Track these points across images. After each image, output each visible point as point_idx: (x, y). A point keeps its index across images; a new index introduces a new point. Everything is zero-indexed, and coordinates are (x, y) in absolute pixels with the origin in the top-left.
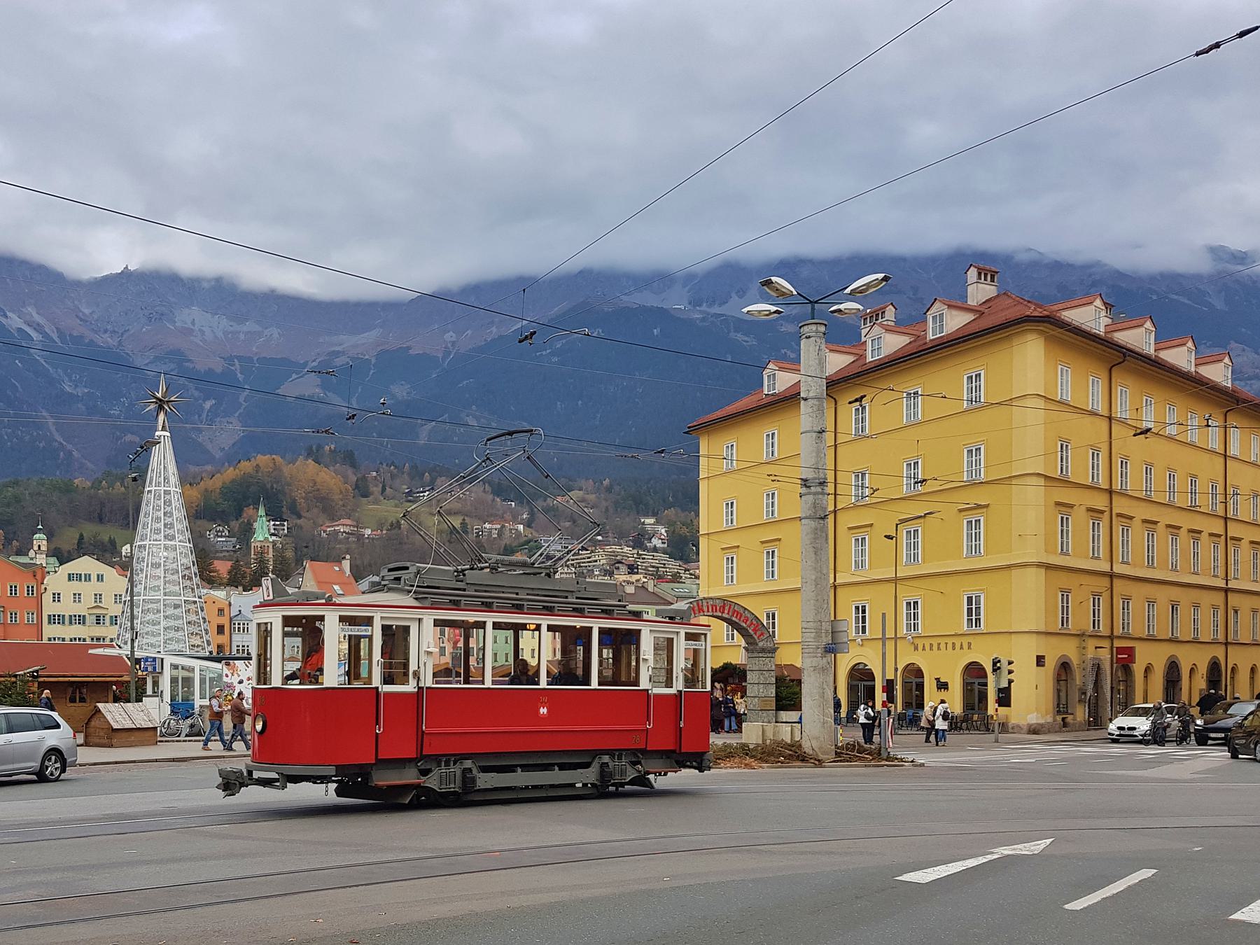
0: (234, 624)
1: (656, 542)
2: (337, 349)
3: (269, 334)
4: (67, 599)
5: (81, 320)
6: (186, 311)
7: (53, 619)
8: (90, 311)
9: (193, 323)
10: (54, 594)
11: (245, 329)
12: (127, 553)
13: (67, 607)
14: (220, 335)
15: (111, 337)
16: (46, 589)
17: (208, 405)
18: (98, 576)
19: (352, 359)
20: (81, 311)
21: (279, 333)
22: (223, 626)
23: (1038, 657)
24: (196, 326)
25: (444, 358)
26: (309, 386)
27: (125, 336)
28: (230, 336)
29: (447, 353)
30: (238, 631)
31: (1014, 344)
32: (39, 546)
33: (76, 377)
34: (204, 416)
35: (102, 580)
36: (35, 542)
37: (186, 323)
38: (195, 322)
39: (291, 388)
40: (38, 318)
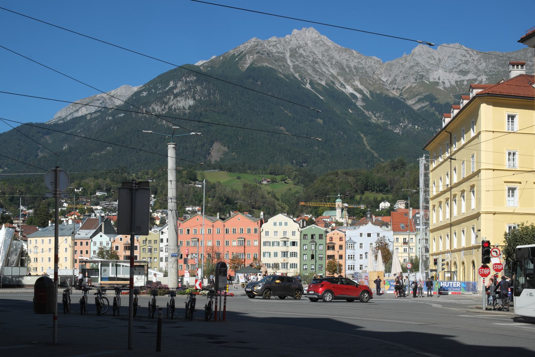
0: (347, 245)
3: (480, 80)
4: (271, 234)
6: (436, 72)
7: (265, 243)
8: (386, 80)
9: (439, 79)
12: (382, 207)
13: (271, 238)
15: (396, 92)
16: (263, 230)
20: (381, 80)
21: (486, 78)
24: (440, 80)
30: (351, 248)
33: (378, 115)
37: (435, 79)
38: (440, 78)
40: (360, 86)
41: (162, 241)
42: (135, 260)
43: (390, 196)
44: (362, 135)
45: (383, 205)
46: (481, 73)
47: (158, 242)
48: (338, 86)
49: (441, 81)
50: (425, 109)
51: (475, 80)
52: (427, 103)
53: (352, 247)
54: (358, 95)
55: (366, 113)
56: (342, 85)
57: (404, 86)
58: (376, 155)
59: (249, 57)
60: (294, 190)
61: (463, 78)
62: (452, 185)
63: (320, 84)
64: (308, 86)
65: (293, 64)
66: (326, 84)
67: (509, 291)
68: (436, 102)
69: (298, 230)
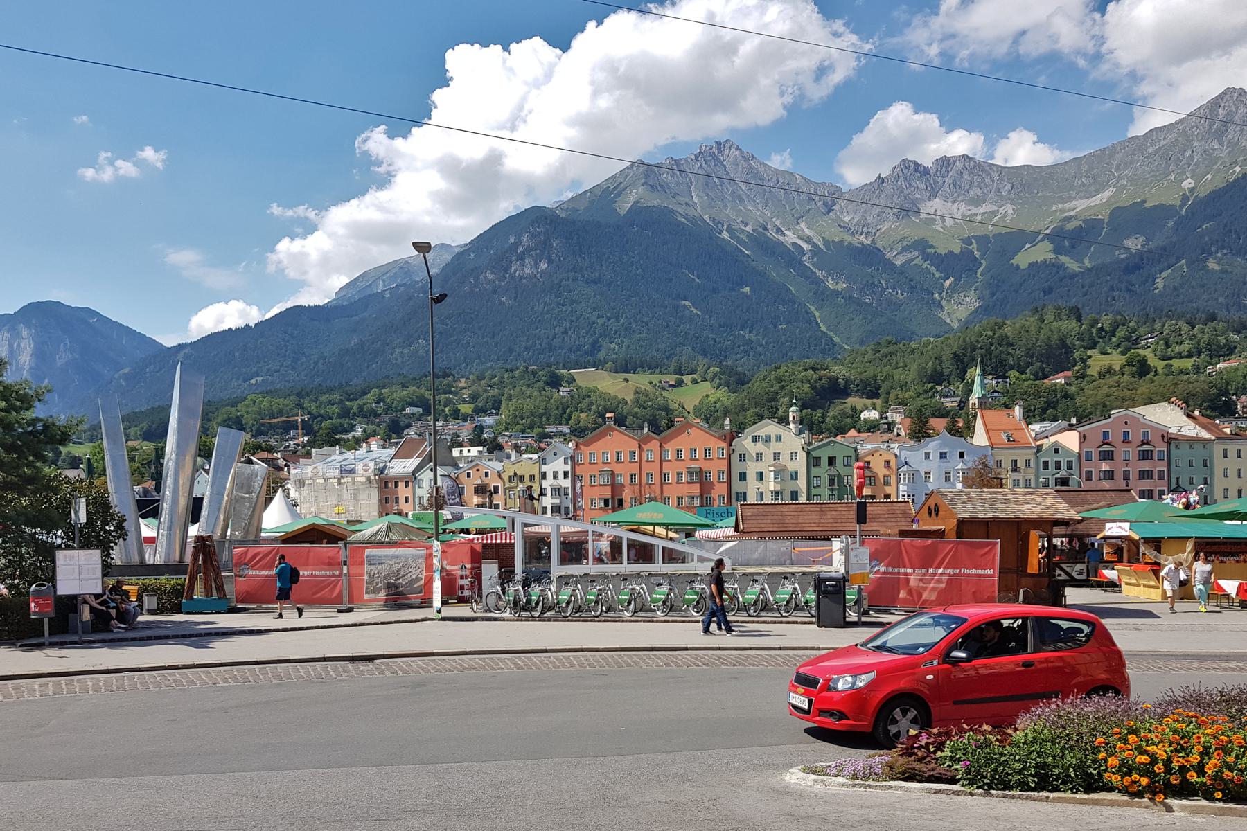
3: (1004, 212)
5: (841, 227)
10: (740, 455)
11: (981, 210)
17: (947, 284)
18: (777, 436)
21: (1013, 209)
23: (745, 480)
25: (1182, 206)
26: (1041, 252)
29: (1185, 198)
32: (794, 417)
34: (944, 293)
35: (780, 440)
36: (790, 414)
41: (544, 476)
43: (878, 402)
44: (813, 309)
45: (867, 416)
47: (537, 478)
48: (772, 233)
51: (995, 213)
52: (917, 254)
53: (909, 478)
54: (805, 246)
55: (818, 273)
56: (778, 230)
57: (879, 227)
58: (836, 339)
59: (631, 192)
60: (712, 399)
63: (743, 231)
64: (725, 235)
65: (701, 200)
66: (753, 230)
68: (933, 251)
69: (803, 448)
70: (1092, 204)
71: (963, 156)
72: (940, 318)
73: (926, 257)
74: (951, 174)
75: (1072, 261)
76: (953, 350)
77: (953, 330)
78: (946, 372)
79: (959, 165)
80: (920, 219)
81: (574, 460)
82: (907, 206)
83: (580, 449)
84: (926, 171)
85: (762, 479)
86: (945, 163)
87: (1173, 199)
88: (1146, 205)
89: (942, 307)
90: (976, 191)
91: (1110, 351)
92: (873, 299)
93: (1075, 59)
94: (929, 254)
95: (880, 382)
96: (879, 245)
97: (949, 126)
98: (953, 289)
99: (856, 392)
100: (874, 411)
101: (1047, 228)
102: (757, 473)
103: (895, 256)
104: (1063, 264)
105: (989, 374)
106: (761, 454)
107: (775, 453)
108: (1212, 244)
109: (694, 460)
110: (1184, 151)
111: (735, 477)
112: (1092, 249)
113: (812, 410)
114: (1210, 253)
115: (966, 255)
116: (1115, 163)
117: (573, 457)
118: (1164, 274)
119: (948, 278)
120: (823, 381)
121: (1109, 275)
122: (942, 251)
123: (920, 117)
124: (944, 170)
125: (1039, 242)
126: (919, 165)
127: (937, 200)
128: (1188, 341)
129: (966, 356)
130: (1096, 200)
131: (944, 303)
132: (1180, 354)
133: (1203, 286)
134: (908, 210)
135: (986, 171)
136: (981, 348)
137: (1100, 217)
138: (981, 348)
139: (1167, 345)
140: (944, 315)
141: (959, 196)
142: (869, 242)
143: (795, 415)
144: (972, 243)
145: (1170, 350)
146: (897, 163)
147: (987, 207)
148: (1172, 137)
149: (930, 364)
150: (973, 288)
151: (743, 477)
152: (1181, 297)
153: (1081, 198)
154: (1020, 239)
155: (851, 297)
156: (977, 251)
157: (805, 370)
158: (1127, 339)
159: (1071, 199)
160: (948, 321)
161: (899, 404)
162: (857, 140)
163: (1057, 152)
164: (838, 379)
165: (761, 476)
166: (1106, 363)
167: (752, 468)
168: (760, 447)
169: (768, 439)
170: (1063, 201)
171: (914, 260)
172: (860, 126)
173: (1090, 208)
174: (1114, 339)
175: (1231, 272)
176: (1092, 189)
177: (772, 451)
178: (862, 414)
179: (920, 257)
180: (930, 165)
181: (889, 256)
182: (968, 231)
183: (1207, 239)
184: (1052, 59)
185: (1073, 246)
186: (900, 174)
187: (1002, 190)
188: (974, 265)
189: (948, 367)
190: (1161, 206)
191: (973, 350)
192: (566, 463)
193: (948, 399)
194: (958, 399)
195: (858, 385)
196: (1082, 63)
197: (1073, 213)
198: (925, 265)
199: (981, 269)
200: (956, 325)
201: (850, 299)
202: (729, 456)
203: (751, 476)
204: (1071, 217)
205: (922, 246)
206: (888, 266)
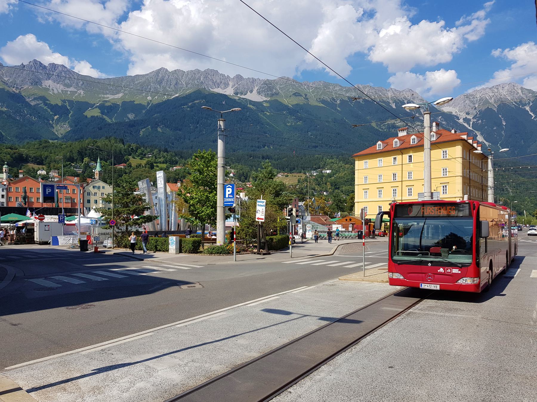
1: (231, 175)
2: (106, 99)
5: (3, 82)
9: (49, 86)
14: (60, 91)
15: (16, 90)
16: (85, 191)
17: (56, 117)
18: (103, 187)
19: (112, 103)
22: (4, 195)
23: (90, 203)
25: (148, 106)
26: (96, 113)
27: (21, 90)
28: (64, 92)
29: (148, 104)
31: (321, 65)
32: (6, 170)
34: (54, 121)
36: (4, 168)
39: (90, 113)
42: (5, 206)
46: (80, 88)
49: (51, 88)
50: (40, 105)
51: (76, 92)
57: (22, 86)
61: (67, 89)
62: (425, 221)
67: (400, 139)
70: (115, 98)
71: (62, 65)
72: (53, 132)
73: (46, 104)
74: (56, 71)
75: (108, 118)
76: (78, 149)
77: (59, 138)
78: (75, 158)
79: (60, 68)
80: (42, 87)
81: (7, 190)
82: (36, 80)
83: (11, 185)
84: (45, 67)
85: (96, 203)
86: (54, 66)
87: (144, 103)
88: (135, 103)
89: (53, 127)
90: (67, 81)
91: (136, 157)
92: (20, 118)
93: (108, 39)
94: (47, 103)
95: (44, 159)
96: (23, 94)
97: (55, 50)
98: (58, 121)
99: (32, 161)
100: (44, 171)
101: (98, 103)
102: (95, 200)
103: (30, 101)
104: (105, 119)
105: (93, 161)
106: (96, 193)
107: (102, 193)
108: (159, 122)
109: (17, 192)
110: (148, 86)
111: (86, 201)
112: (115, 115)
113: (12, 167)
114: (158, 125)
115: (63, 107)
116: (123, 84)
117: (7, 189)
118: (143, 130)
119: (56, 115)
120: (16, 155)
121: (123, 127)
122: (53, 103)
123: (41, 44)
124: (53, 69)
125: (95, 108)
126: (42, 64)
127: (50, 81)
128: (162, 158)
129: (83, 152)
130: (117, 96)
131: (54, 125)
132: (160, 162)
133: (156, 137)
134: (36, 82)
135: (72, 74)
136: (89, 150)
137: (118, 103)
138: (89, 150)
139: (156, 158)
140: (54, 131)
141: (60, 81)
142: (17, 92)
143: (6, 169)
144: (66, 103)
145: (157, 160)
146: (32, 60)
147: (72, 89)
148: (144, 79)
149: (68, 154)
150: (67, 122)
151: (89, 201)
152: (149, 139)
153: (111, 94)
154: (87, 105)
155: (10, 115)
156: (69, 106)
157: (7, 149)
158: (142, 154)
159: (107, 94)
160: (56, 133)
161: (55, 169)
162: (9, 44)
163: (100, 73)
164: (23, 154)
165: (96, 202)
166: (139, 162)
167: (92, 198)
168: (96, 190)
169: (99, 188)
170: (104, 94)
171: (40, 104)
172: (13, 38)
173: (114, 99)
174: (137, 153)
175: (165, 133)
176: (115, 92)
177: (101, 192)
178: (38, 172)
179: (43, 104)
180: (47, 65)
181: (27, 100)
182: (64, 98)
183: (157, 120)
184: (99, 36)
185: (108, 112)
186: (33, 65)
187: (79, 84)
188: (67, 112)
189: (75, 156)
190: (140, 104)
191: (86, 150)
192: (3, 191)
193: (77, 169)
194: (82, 170)
195: (32, 158)
196: (111, 42)
197: (107, 99)
198: (45, 108)
199: (71, 114)
200: (60, 136)
201: (9, 116)
202: (83, 193)
203: (92, 201)
204: (107, 101)
205: (44, 99)
206: (28, 105)
